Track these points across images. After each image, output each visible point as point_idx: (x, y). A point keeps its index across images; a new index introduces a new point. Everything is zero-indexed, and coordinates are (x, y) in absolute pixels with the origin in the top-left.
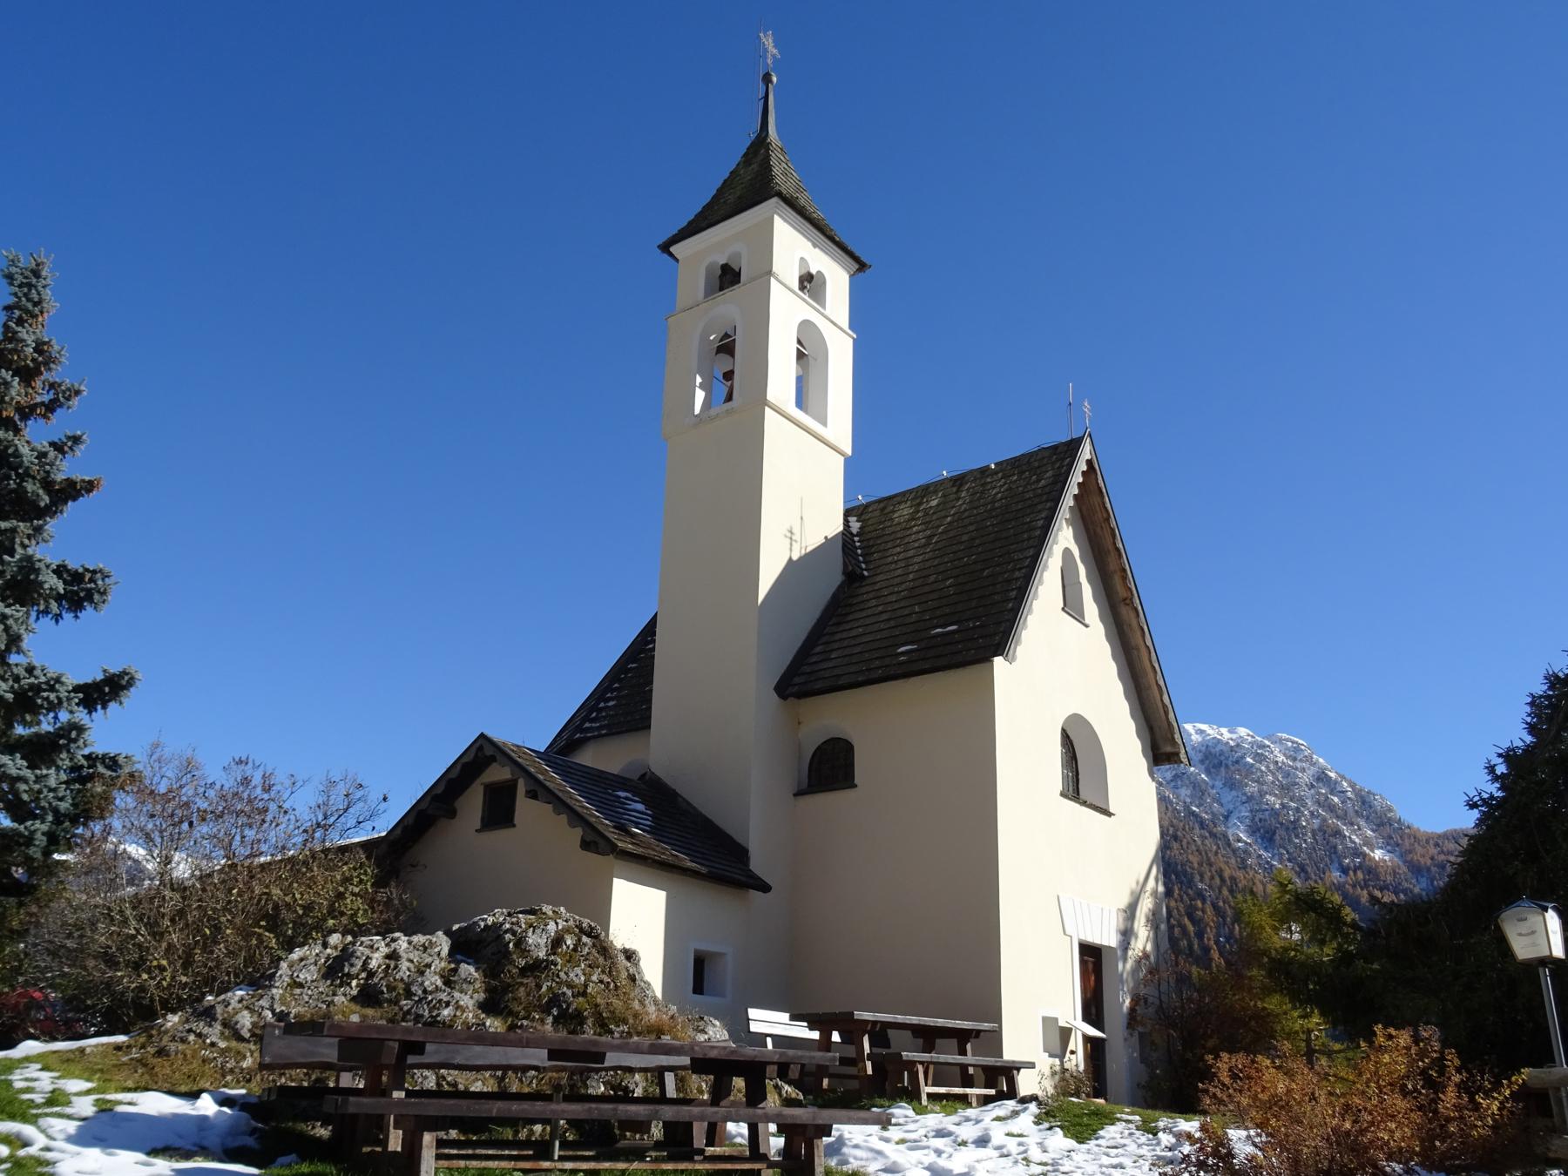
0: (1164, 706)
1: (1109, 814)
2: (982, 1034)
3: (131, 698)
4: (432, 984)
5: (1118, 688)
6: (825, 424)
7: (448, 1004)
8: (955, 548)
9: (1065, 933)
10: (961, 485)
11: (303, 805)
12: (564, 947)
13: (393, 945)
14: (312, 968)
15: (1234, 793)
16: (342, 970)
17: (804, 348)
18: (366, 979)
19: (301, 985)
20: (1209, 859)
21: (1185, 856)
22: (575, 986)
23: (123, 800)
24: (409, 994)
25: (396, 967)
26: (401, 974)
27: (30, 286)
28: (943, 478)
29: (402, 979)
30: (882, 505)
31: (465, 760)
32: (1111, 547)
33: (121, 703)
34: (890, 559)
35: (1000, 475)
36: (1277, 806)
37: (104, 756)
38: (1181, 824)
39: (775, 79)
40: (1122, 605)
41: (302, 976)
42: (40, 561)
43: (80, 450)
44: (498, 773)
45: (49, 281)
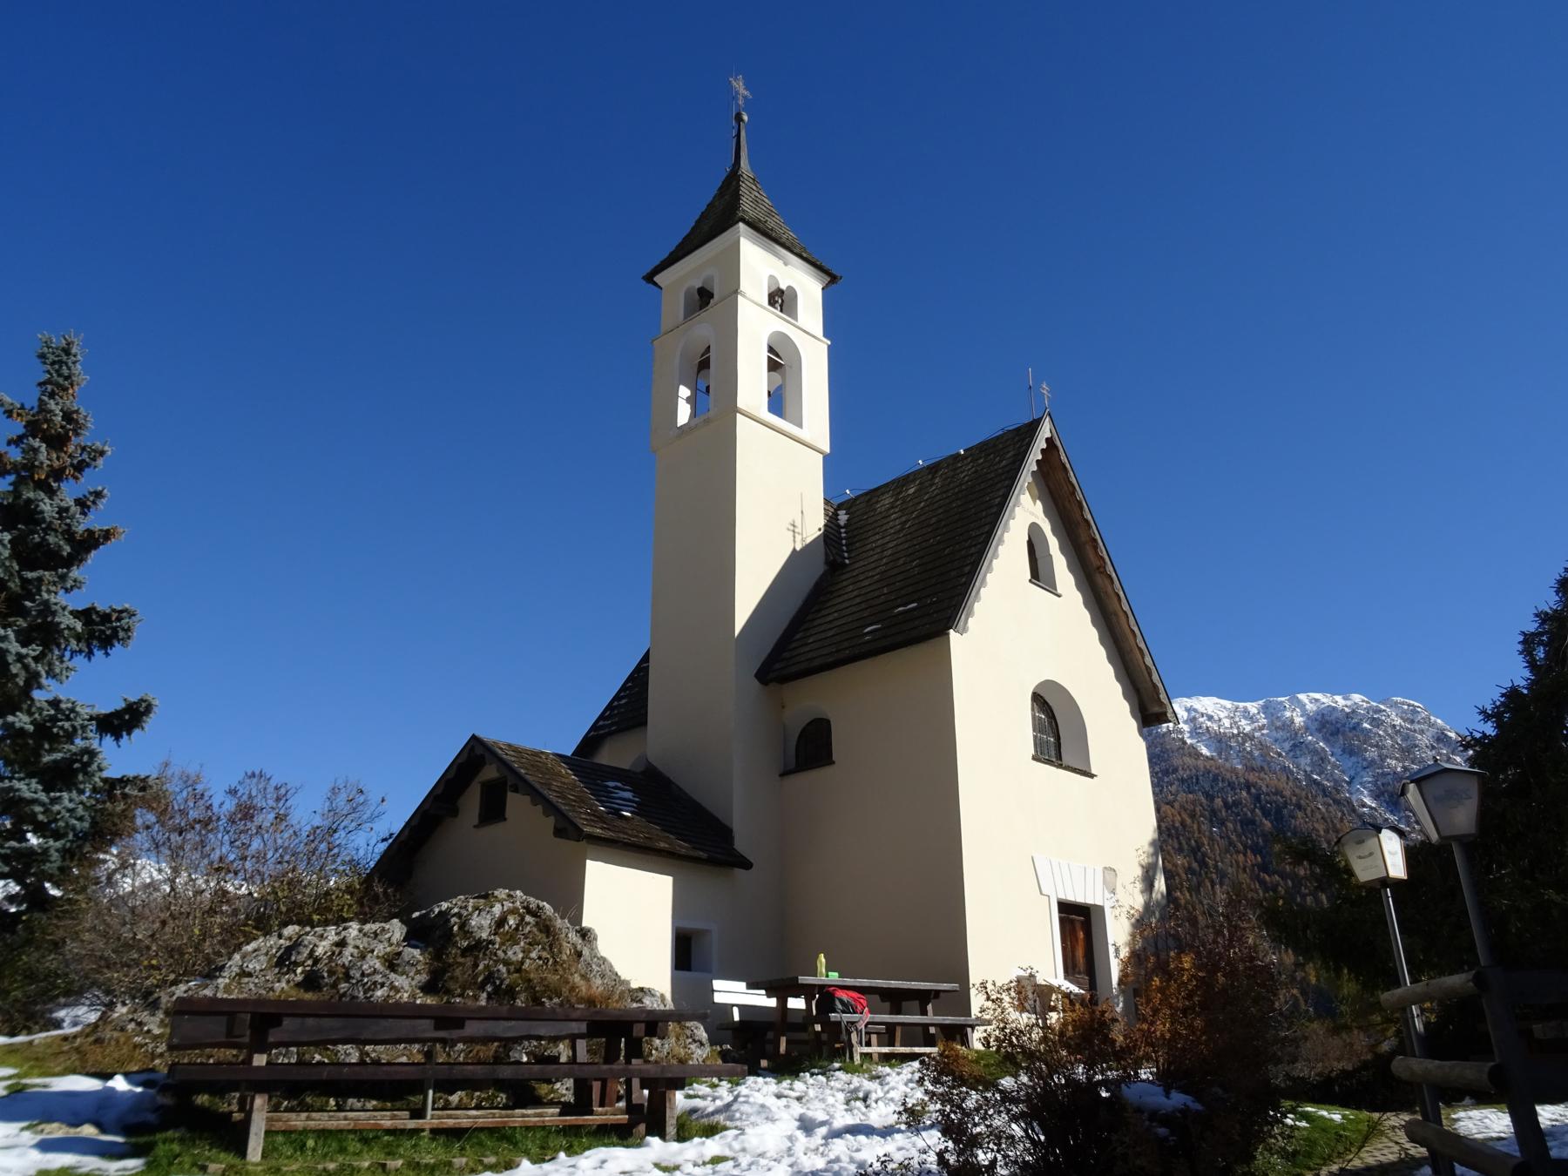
0: (1147, 668)
1: (1092, 776)
2: (941, 994)
3: (150, 722)
4: (370, 967)
5: (1101, 652)
6: (800, 425)
7: (382, 985)
8: (924, 531)
9: (1041, 893)
10: (936, 472)
11: (306, 813)
12: (507, 927)
13: (343, 933)
14: (262, 958)
15: (1354, 759)
16: (289, 958)
17: (778, 356)
18: (313, 966)
19: (250, 975)
20: (1334, 826)
21: (1310, 824)
22: (512, 963)
23: (143, 817)
24: (347, 977)
25: (340, 953)
26: (344, 960)
27: (61, 362)
28: (917, 468)
29: (344, 965)
30: (868, 497)
31: (459, 761)
32: (1080, 519)
33: (143, 729)
34: (869, 547)
35: (969, 460)
36: (1399, 769)
37: (135, 778)
38: (1304, 793)
39: (745, 118)
40: (1098, 575)
41: (251, 966)
42: (56, 604)
43: (102, 503)
44: (490, 772)
45: (79, 357)
